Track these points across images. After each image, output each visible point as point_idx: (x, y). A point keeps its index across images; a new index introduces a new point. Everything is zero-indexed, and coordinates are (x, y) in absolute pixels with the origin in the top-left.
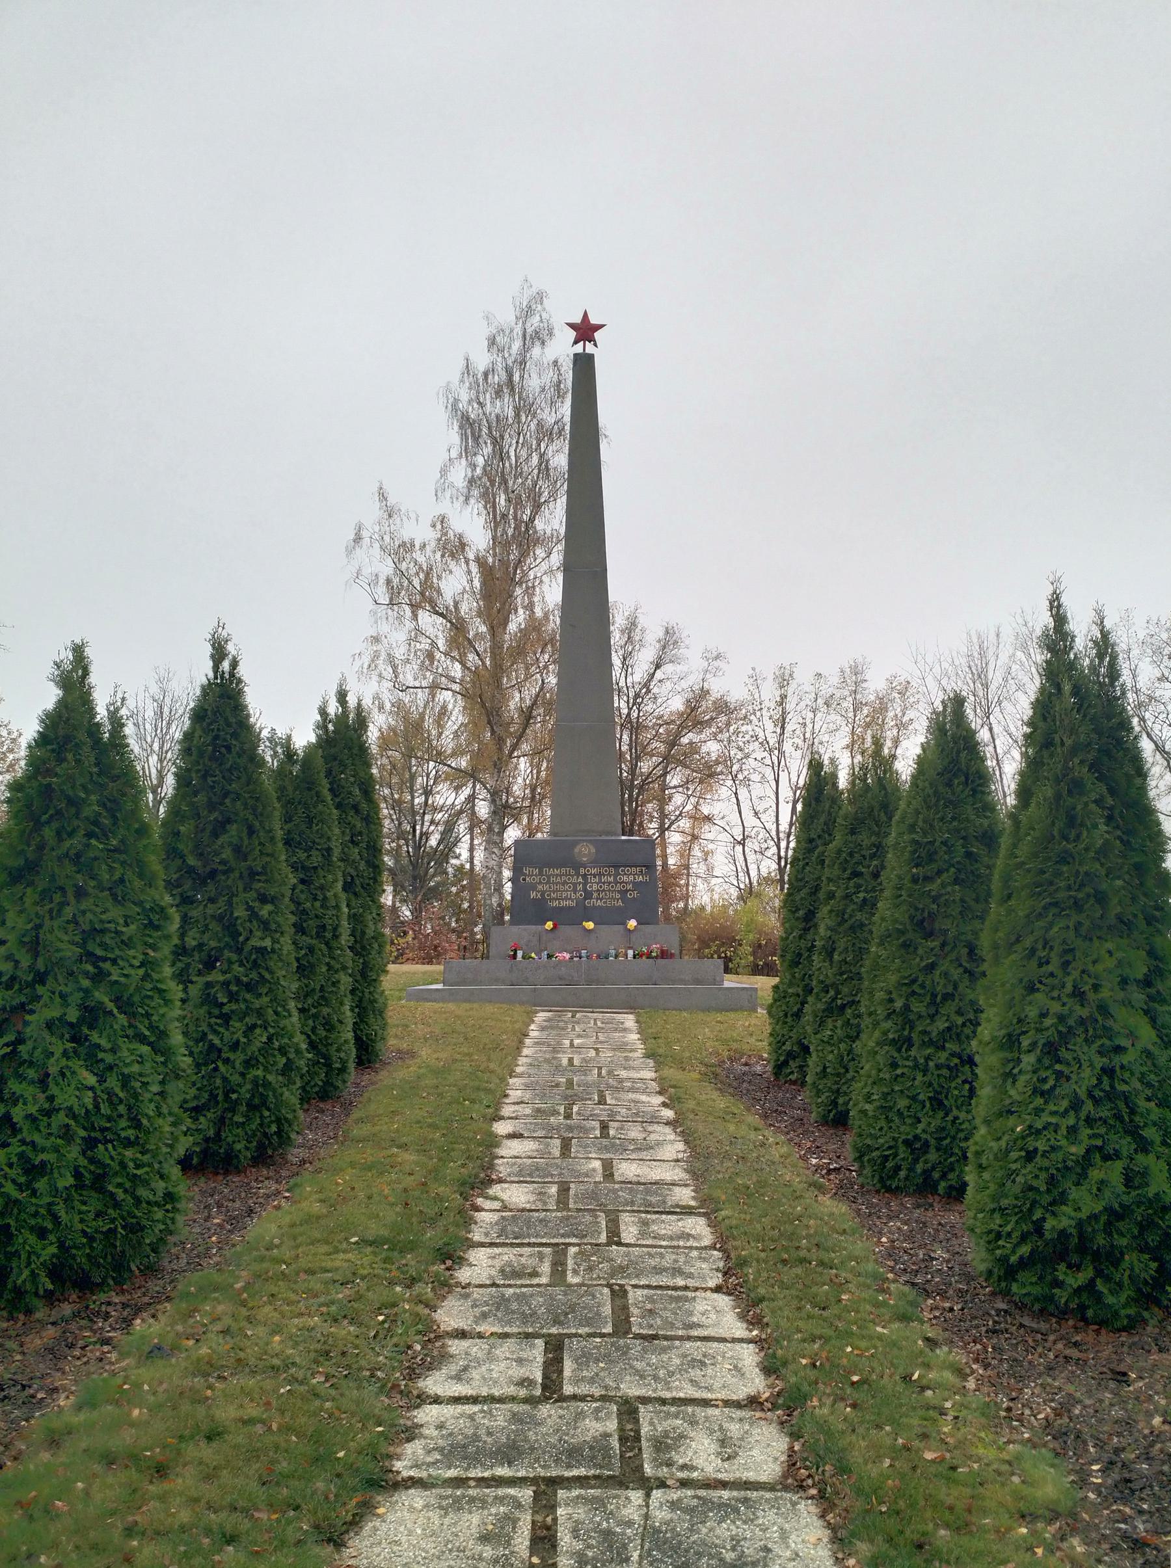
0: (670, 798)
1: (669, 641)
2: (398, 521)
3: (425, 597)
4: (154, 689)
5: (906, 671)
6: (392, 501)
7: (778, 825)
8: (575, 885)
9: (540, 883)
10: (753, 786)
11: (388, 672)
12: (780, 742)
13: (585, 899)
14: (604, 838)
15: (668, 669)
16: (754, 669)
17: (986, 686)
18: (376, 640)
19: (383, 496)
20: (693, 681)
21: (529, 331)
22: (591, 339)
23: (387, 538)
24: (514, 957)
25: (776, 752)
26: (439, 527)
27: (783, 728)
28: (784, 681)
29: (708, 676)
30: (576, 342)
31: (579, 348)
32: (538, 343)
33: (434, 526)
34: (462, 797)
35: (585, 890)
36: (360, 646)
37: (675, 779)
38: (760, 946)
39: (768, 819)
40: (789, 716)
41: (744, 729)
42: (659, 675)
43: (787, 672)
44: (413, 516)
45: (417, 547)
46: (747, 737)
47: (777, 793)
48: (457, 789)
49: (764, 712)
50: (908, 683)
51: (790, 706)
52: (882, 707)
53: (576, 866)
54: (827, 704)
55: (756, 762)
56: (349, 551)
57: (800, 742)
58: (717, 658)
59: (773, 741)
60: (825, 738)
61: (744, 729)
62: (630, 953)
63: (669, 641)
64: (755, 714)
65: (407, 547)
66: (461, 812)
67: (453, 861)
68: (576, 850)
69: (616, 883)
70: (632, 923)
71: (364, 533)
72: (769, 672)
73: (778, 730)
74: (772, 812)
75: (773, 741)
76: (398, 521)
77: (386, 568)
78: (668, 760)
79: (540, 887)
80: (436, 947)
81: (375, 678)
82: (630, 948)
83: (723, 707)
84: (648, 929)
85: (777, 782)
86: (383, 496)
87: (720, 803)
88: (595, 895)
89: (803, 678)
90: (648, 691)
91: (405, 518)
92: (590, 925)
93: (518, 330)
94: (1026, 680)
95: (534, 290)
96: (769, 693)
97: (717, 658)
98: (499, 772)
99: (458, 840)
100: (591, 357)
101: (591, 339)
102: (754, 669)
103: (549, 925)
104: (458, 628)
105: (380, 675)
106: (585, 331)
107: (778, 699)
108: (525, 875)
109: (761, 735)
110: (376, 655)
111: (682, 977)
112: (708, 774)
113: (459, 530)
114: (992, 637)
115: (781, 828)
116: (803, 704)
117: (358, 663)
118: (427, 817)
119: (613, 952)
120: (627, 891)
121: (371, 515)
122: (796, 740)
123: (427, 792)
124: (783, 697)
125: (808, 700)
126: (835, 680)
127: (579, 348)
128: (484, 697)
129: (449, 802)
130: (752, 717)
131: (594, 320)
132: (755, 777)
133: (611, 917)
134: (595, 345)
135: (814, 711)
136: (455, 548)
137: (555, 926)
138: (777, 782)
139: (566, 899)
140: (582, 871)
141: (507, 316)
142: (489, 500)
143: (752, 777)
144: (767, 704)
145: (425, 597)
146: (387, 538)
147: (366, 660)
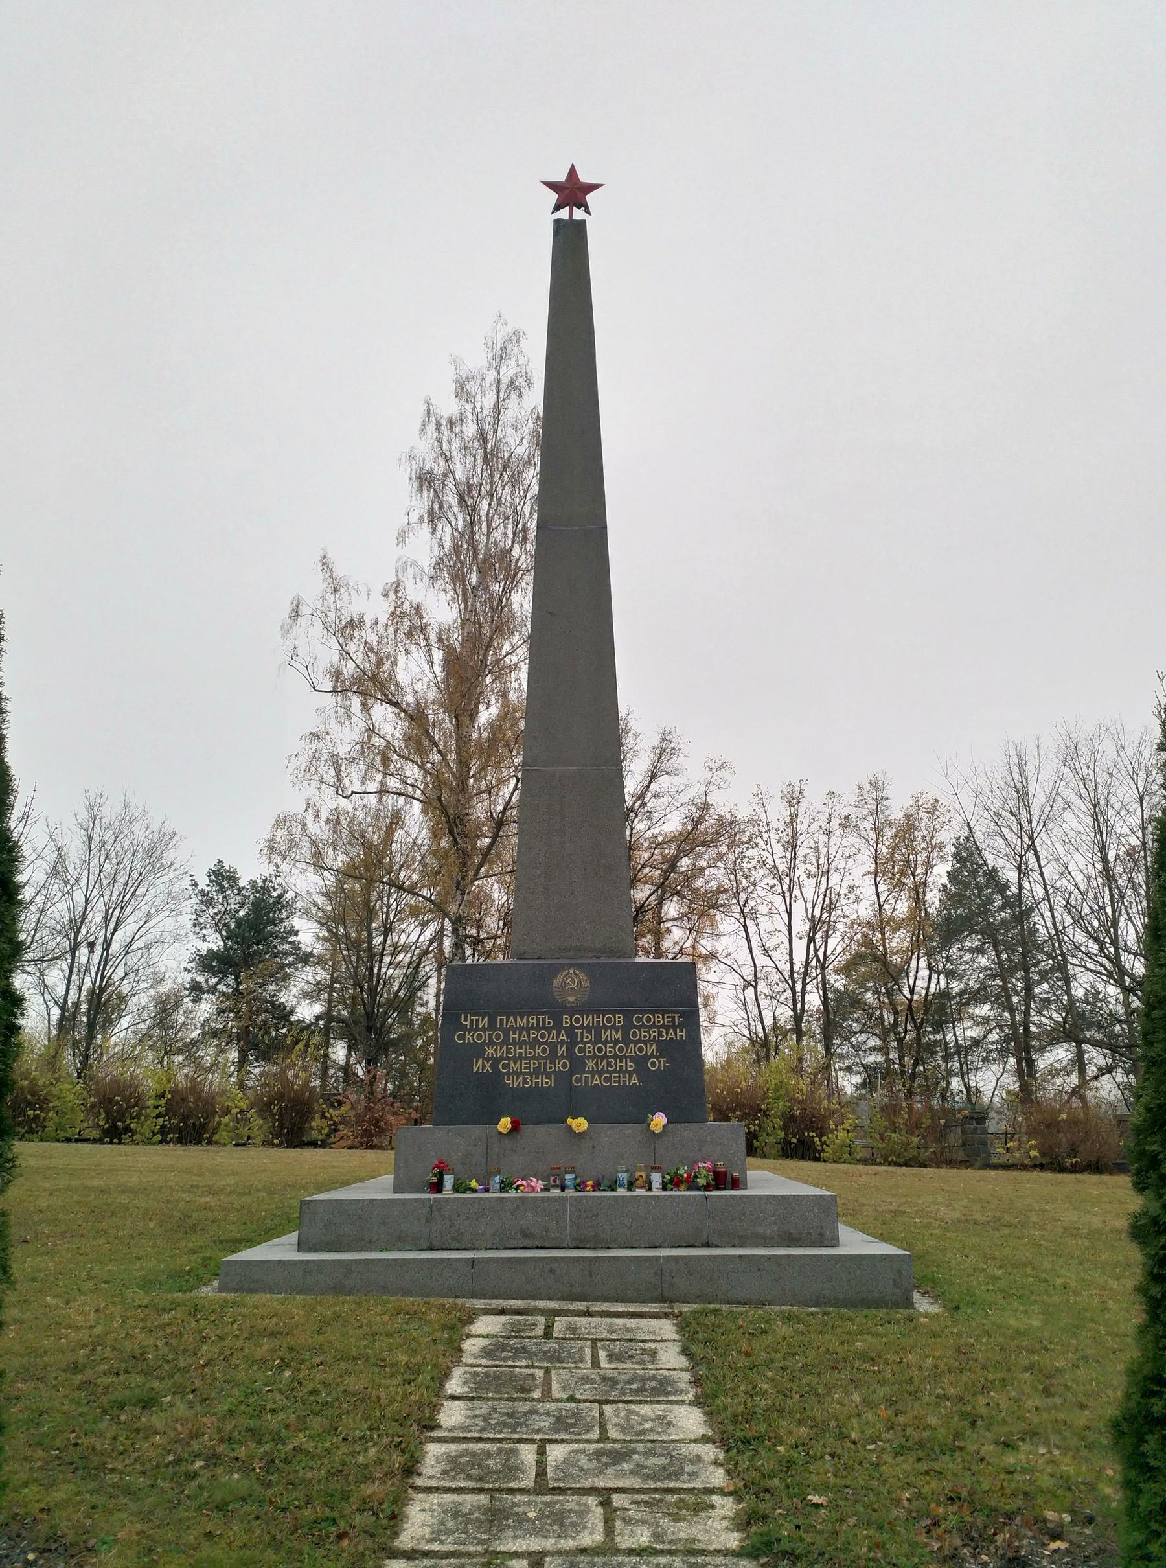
0: (668, 931)
1: (665, 751)
2: (345, 596)
3: (373, 685)
4: (84, 815)
5: (934, 788)
6: (338, 572)
7: (792, 964)
8: (553, 1047)
9: (491, 1043)
10: (761, 919)
11: (330, 776)
12: (792, 867)
13: (571, 1072)
14: (603, 960)
15: (663, 783)
16: (758, 786)
17: (1028, 806)
18: (315, 736)
19: (325, 563)
20: (694, 792)
21: (505, 381)
22: (583, 205)
23: (332, 616)
24: (438, 1187)
25: (787, 880)
26: (392, 596)
27: (794, 851)
28: (793, 799)
29: (711, 788)
30: (557, 208)
31: (564, 214)
32: (514, 396)
33: (386, 595)
34: (428, 934)
35: (570, 1055)
36: (299, 745)
37: (672, 908)
38: (792, 1116)
39: (781, 956)
40: (801, 839)
41: (748, 853)
42: (654, 787)
43: (797, 790)
44: (363, 589)
45: (368, 624)
46: (754, 862)
47: (790, 927)
48: (424, 925)
49: (772, 832)
50: (937, 800)
51: (801, 828)
52: (909, 826)
53: (556, 1011)
54: (843, 825)
55: (765, 896)
56: (285, 631)
57: (813, 869)
58: (723, 766)
59: (783, 867)
60: (842, 865)
61: (748, 853)
62: (657, 1178)
63: (665, 751)
64: (761, 837)
65: (354, 625)
66: (426, 952)
67: (419, 1009)
68: (557, 982)
69: (626, 1040)
70: (659, 1120)
71: (305, 610)
72: (775, 790)
73: (788, 855)
74: (784, 949)
75: (783, 867)
76: (345, 596)
77: (327, 653)
78: (664, 890)
79: (490, 1051)
80: (378, 1121)
81: (315, 784)
82: (656, 1169)
83: (729, 829)
84: (688, 1131)
85: (789, 914)
86: (325, 563)
87: (726, 936)
88: (590, 1064)
89: (813, 800)
90: (644, 804)
91: (353, 592)
92: (580, 1124)
93: (491, 376)
94: (1073, 798)
95: (509, 329)
96: (777, 813)
97: (723, 766)
98: (463, 894)
99: (424, 985)
100: (582, 224)
101: (583, 205)
102: (758, 786)
103: (505, 1123)
104: (416, 717)
105: (322, 781)
106: (572, 192)
107: (788, 819)
108: (464, 1028)
109: (770, 862)
110: (314, 758)
111: (760, 1230)
112: (704, 908)
113: (415, 601)
114: (1032, 751)
115: (796, 968)
116: (815, 825)
117: (292, 766)
118: (387, 959)
119: (624, 1177)
120: (646, 1058)
121: (313, 589)
122: (808, 866)
123: (387, 930)
124: (794, 818)
125: (822, 821)
126: (853, 798)
127: (564, 214)
128: (448, 811)
129: (413, 938)
130: (759, 840)
131: (584, 178)
132: (763, 909)
133: (625, 1108)
134: (588, 212)
135: (829, 833)
136: (410, 622)
137: (516, 1126)
138: (789, 914)
139: (537, 1072)
140: (566, 1020)
141: (476, 360)
142: (458, 578)
143: (760, 908)
144: (775, 824)
145: (373, 685)
146: (332, 616)
147: (303, 761)
